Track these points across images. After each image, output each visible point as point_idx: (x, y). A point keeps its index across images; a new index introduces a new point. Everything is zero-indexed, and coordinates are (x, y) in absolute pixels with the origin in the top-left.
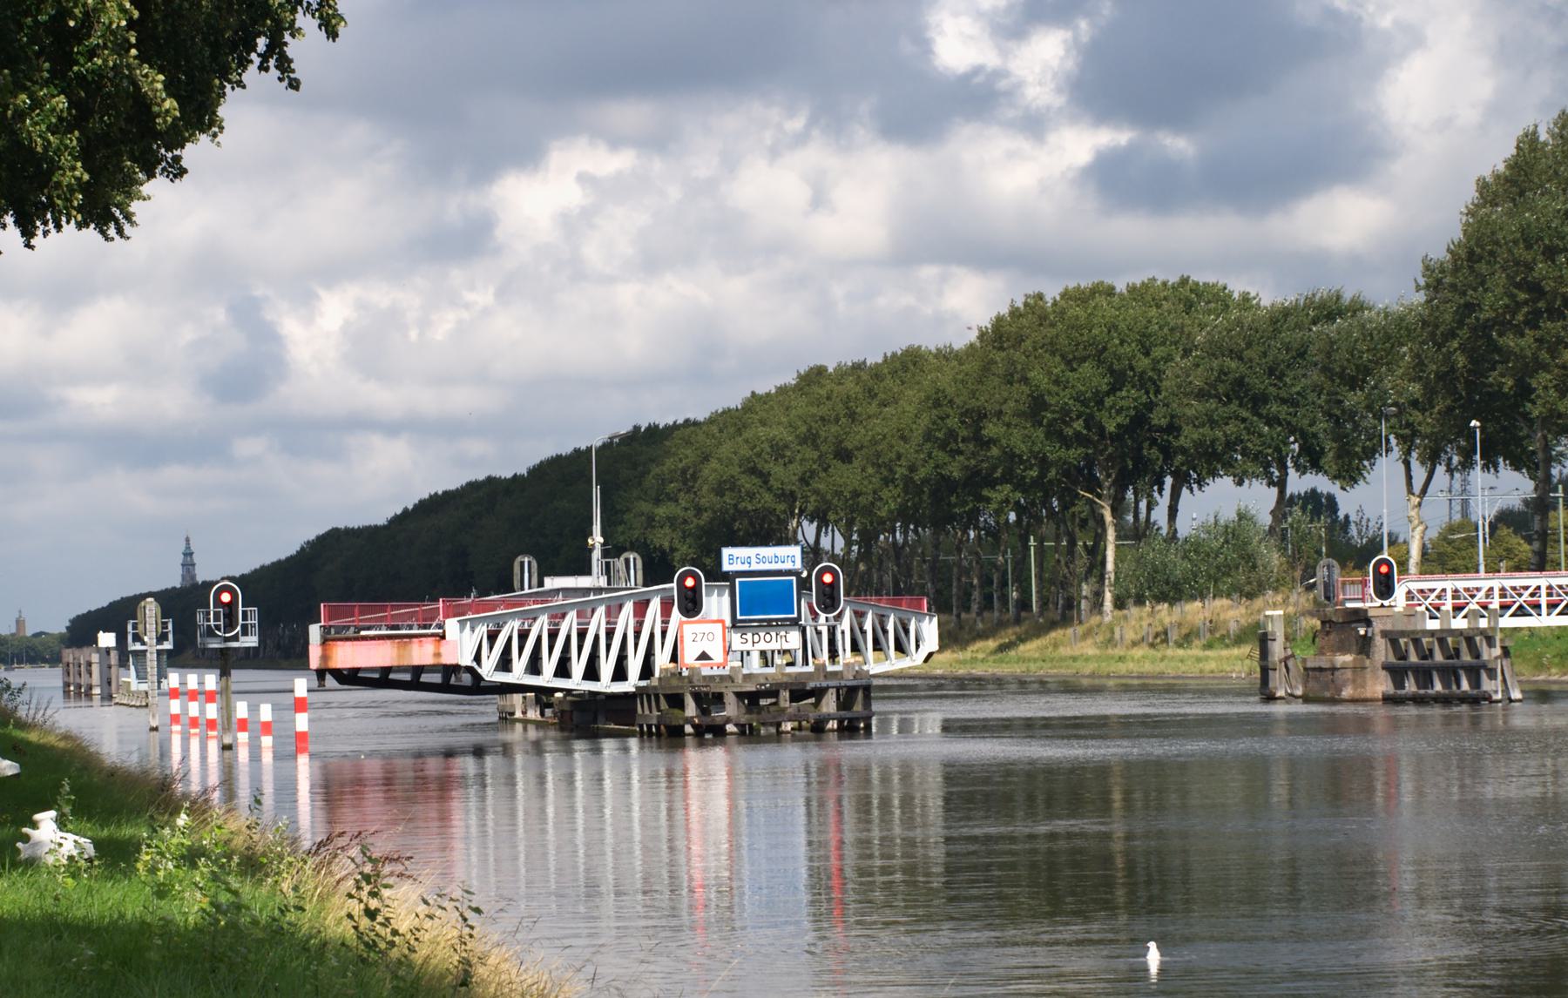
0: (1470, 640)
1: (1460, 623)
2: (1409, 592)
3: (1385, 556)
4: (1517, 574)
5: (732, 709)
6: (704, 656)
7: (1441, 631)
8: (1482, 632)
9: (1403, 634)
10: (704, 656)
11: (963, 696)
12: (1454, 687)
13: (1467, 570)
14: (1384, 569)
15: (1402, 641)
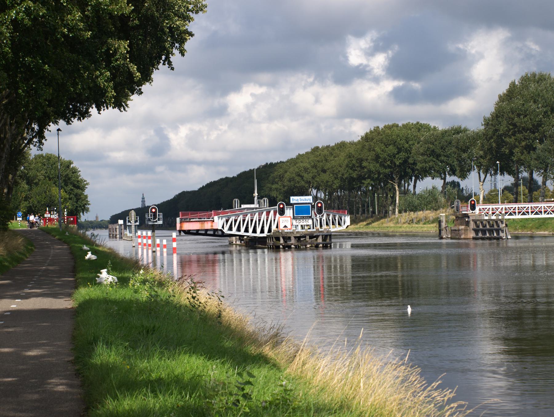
0: (497, 222)
1: (494, 217)
2: (480, 209)
3: (473, 199)
4: (509, 204)
5: (293, 241)
6: (285, 227)
7: (489, 219)
8: (500, 220)
9: (478, 220)
10: (285, 227)
11: (357, 237)
12: (492, 235)
13: (496, 203)
14: (473, 203)
15: (478, 222)
